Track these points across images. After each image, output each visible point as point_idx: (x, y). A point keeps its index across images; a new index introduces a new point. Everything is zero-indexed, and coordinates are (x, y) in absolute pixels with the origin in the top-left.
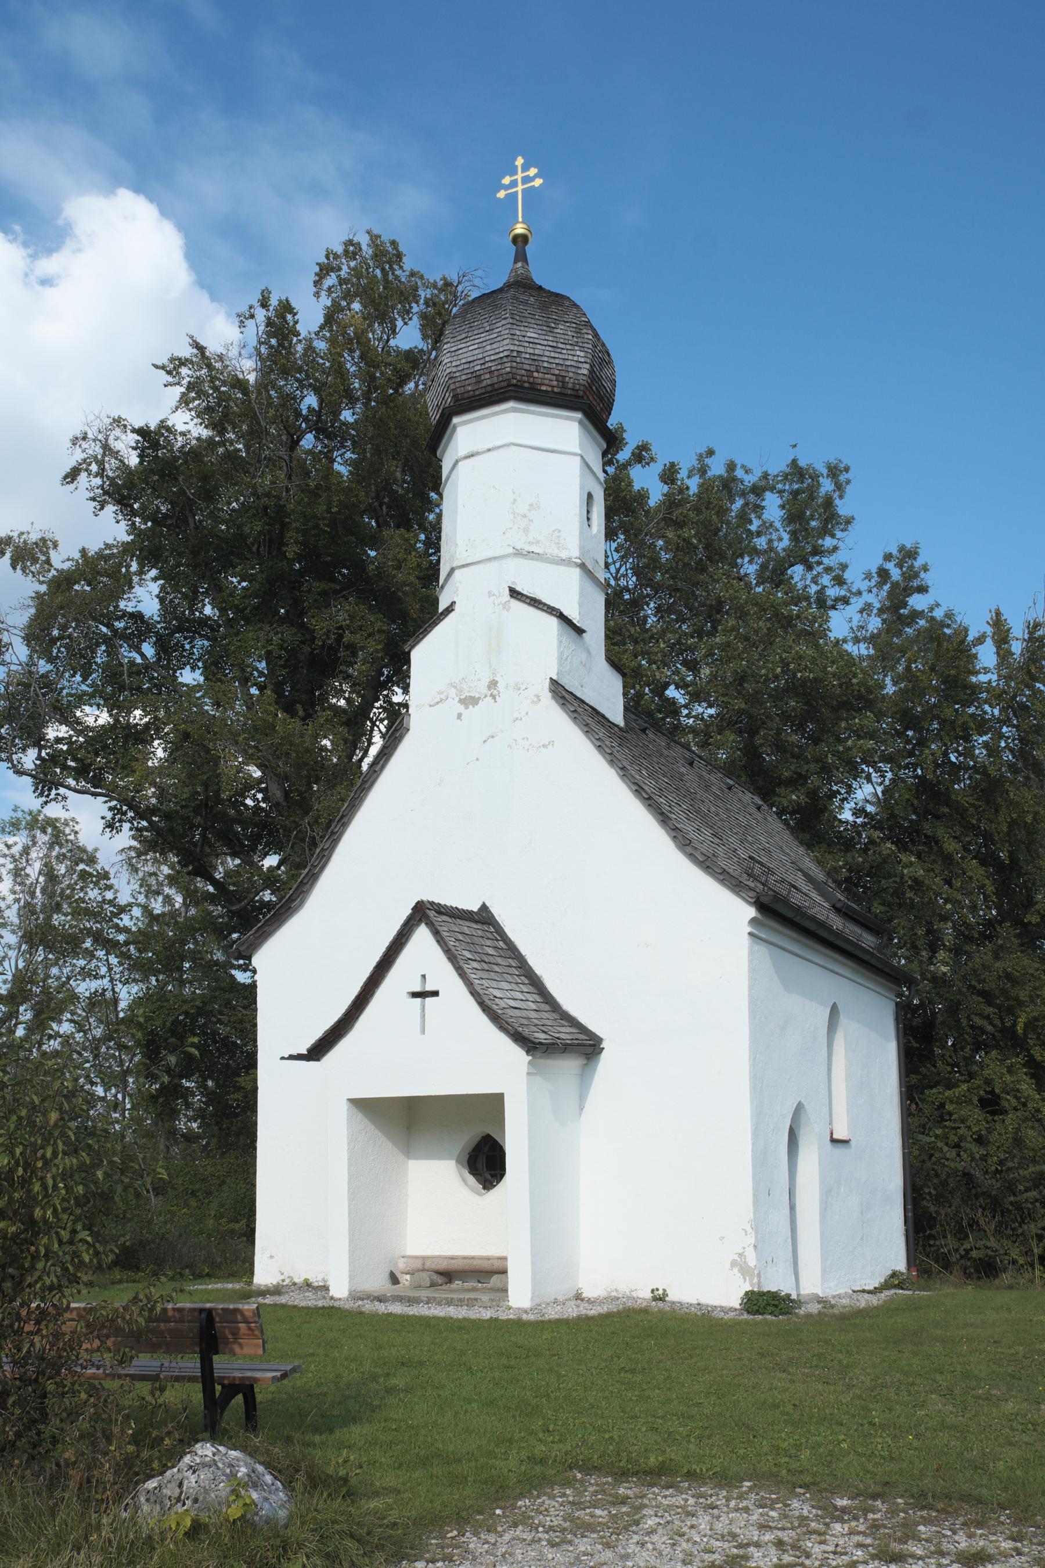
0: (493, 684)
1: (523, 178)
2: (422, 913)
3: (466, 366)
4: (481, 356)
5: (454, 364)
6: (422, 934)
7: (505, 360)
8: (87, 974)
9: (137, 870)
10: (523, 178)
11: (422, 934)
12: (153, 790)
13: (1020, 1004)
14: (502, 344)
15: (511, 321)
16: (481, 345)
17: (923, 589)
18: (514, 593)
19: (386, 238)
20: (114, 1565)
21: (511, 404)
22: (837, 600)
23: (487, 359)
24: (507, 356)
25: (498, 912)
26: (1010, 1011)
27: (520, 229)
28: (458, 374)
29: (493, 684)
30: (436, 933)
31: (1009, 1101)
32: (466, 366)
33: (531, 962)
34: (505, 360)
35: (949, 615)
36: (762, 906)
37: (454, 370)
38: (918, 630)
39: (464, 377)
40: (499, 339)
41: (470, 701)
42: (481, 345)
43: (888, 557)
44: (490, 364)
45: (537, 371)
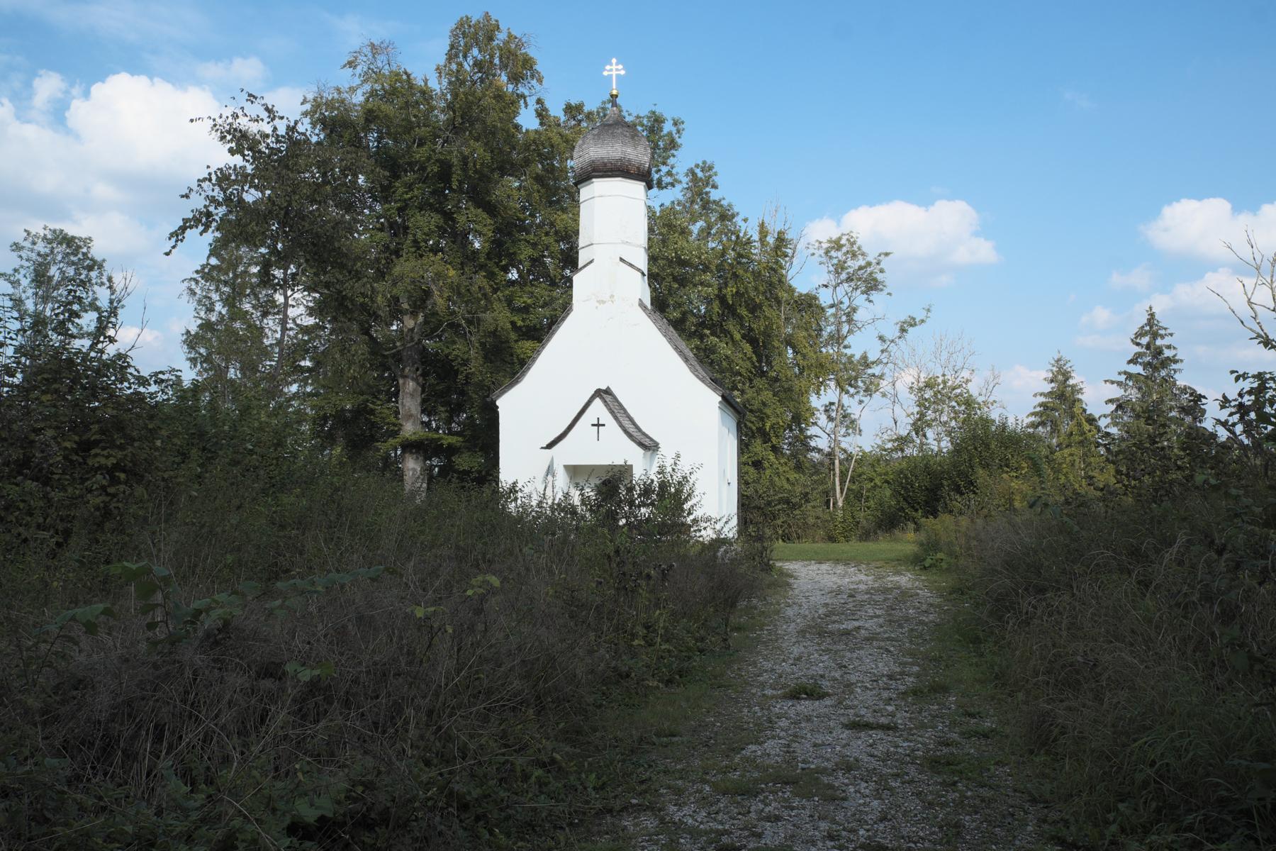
0: (612, 296)
1: (614, 69)
2: (599, 393)
6: (598, 401)
9: (195, 294)
10: (614, 69)
11: (598, 401)
13: (768, 417)
17: (714, 187)
18: (621, 259)
19: (494, 17)
22: (667, 184)
25: (614, 390)
26: (762, 419)
27: (615, 92)
29: (612, 296)
30: (605, 402)
31: (766, 464)
33: (629, 411)
35: (730, 205)
36: (723, 397)
41: (601, 302)
43: (697, 166)
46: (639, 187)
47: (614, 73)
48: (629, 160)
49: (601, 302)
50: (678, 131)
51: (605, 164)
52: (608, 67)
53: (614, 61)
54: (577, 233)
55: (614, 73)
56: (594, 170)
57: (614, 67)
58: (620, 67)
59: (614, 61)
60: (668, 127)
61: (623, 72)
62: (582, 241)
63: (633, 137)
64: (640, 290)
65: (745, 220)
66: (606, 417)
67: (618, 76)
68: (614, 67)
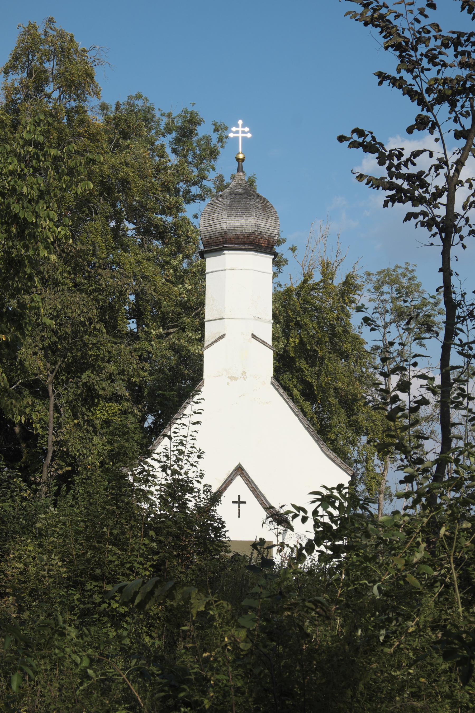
0: (244, 373)
11: (239, 480)
18: (253, 336)
29: (244, 373)
41: (233, 378)
46: (266, 261)
47: (240, 135)
48: (261, 234)
49: (233, 378)
50: (220, 139)
51: (237, 237)
52: (234, 129)
53: (240, 122)
54: (202, 304)
55: (240, 135)
56: (226, 242)
57: (240, 129)
58: (247, 129)
59: (240, 122)
60: (203, 131)
61: (249, 135)
62: (208, 314)
63: (264, 210)
64: (265, 360)
65: (293, 249)
66: (247, 495)
67: (244, 139)
68: (240, 129)
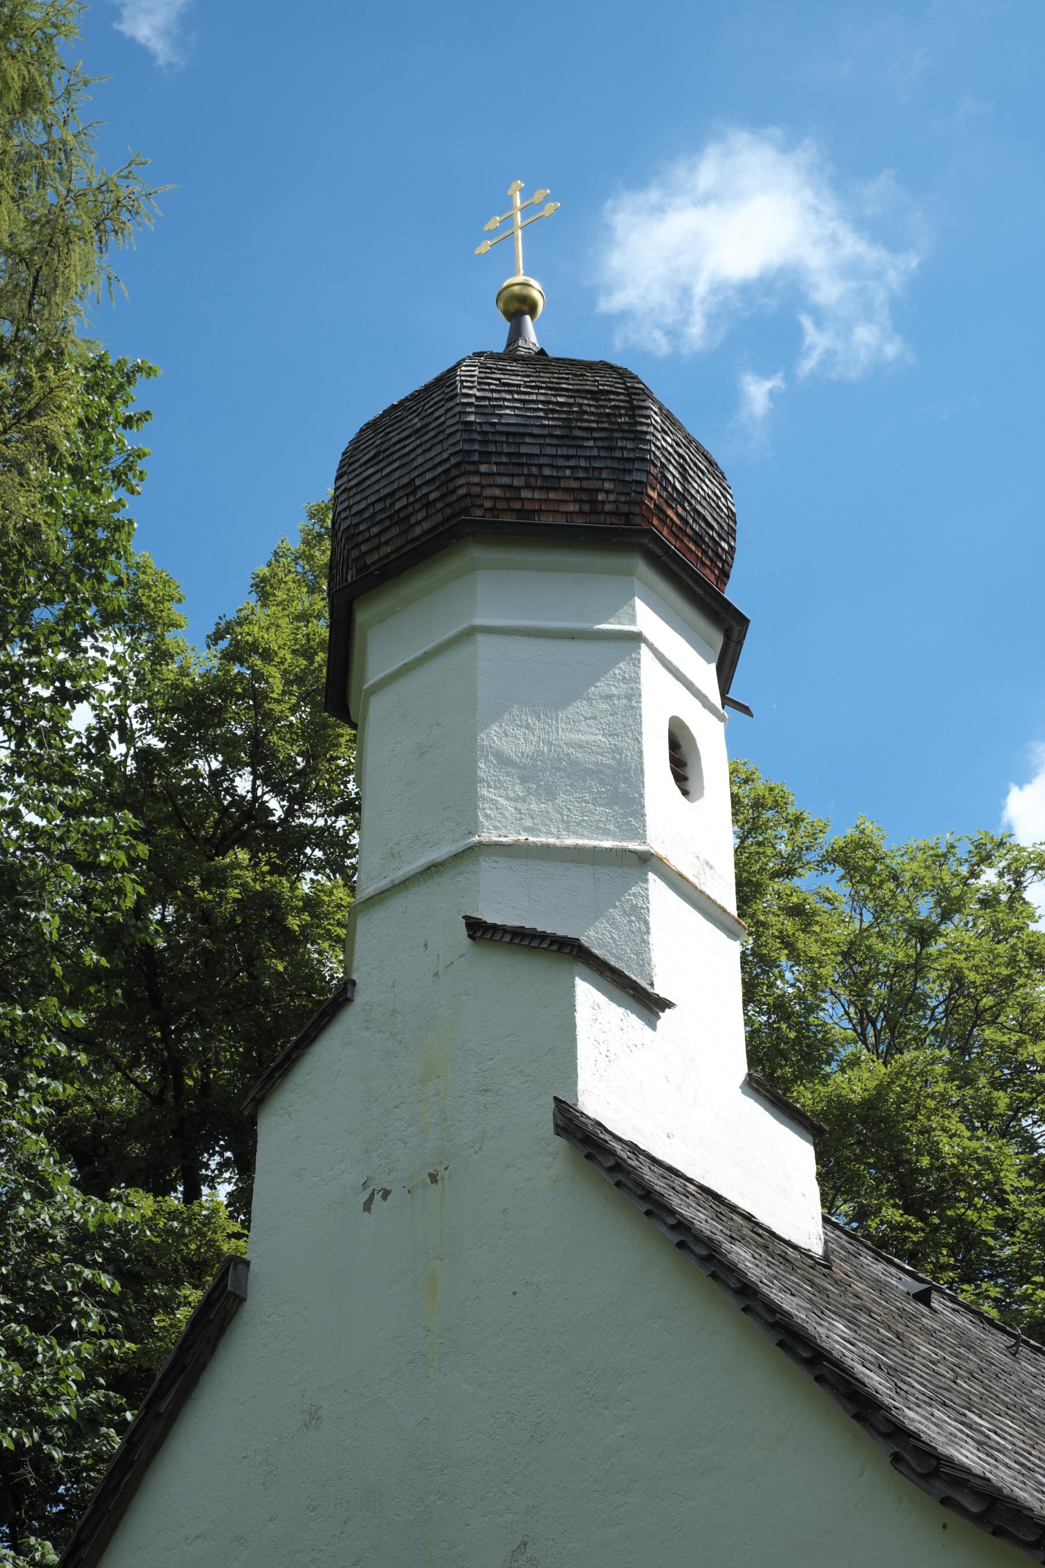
3: (379, 506)
4: (406, 480)
5: (355, 510)
7: (454, 472)
8: (988, 1149)
12: (309, 946)
14: (446, 445)
15: (465, 436)
16: (406, 460)
20: (2, 1243)
21: (477, 553)
23: (418, 482)
24: (457, 465)
28: (362, 527)
32: (379, 506)
34: (454, 472)
37: (355, 521)
38: (71, 1059)
39: (375, 530)
40: (441, 437)
42: (406, 460)
44: (425, 490)
45: (528, 487)
